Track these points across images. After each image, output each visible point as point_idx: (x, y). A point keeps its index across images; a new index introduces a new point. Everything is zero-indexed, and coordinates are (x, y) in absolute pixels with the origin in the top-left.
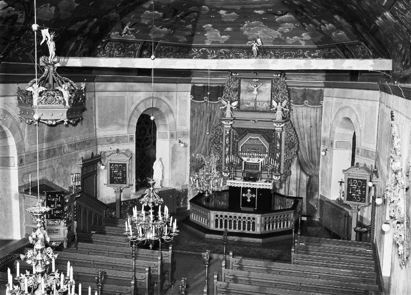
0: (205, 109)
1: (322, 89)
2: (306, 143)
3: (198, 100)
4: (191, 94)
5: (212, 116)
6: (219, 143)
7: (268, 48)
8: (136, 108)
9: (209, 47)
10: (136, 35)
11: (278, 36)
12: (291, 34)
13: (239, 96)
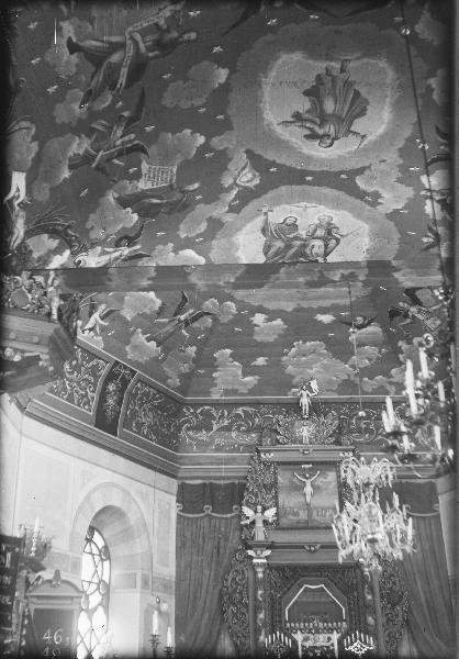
0: (206, 531)
1: (433, 480)
2: (422, 594)
3: (193, 513)
4: (177, 501)
5: (222, 544)
6: (240, 602)
7: (327, 403)
8: (88, 498)
9: (217, 404)
10: (105, 339)
11: (349, 376)
12: (369, 372)
13: (276, 497)
